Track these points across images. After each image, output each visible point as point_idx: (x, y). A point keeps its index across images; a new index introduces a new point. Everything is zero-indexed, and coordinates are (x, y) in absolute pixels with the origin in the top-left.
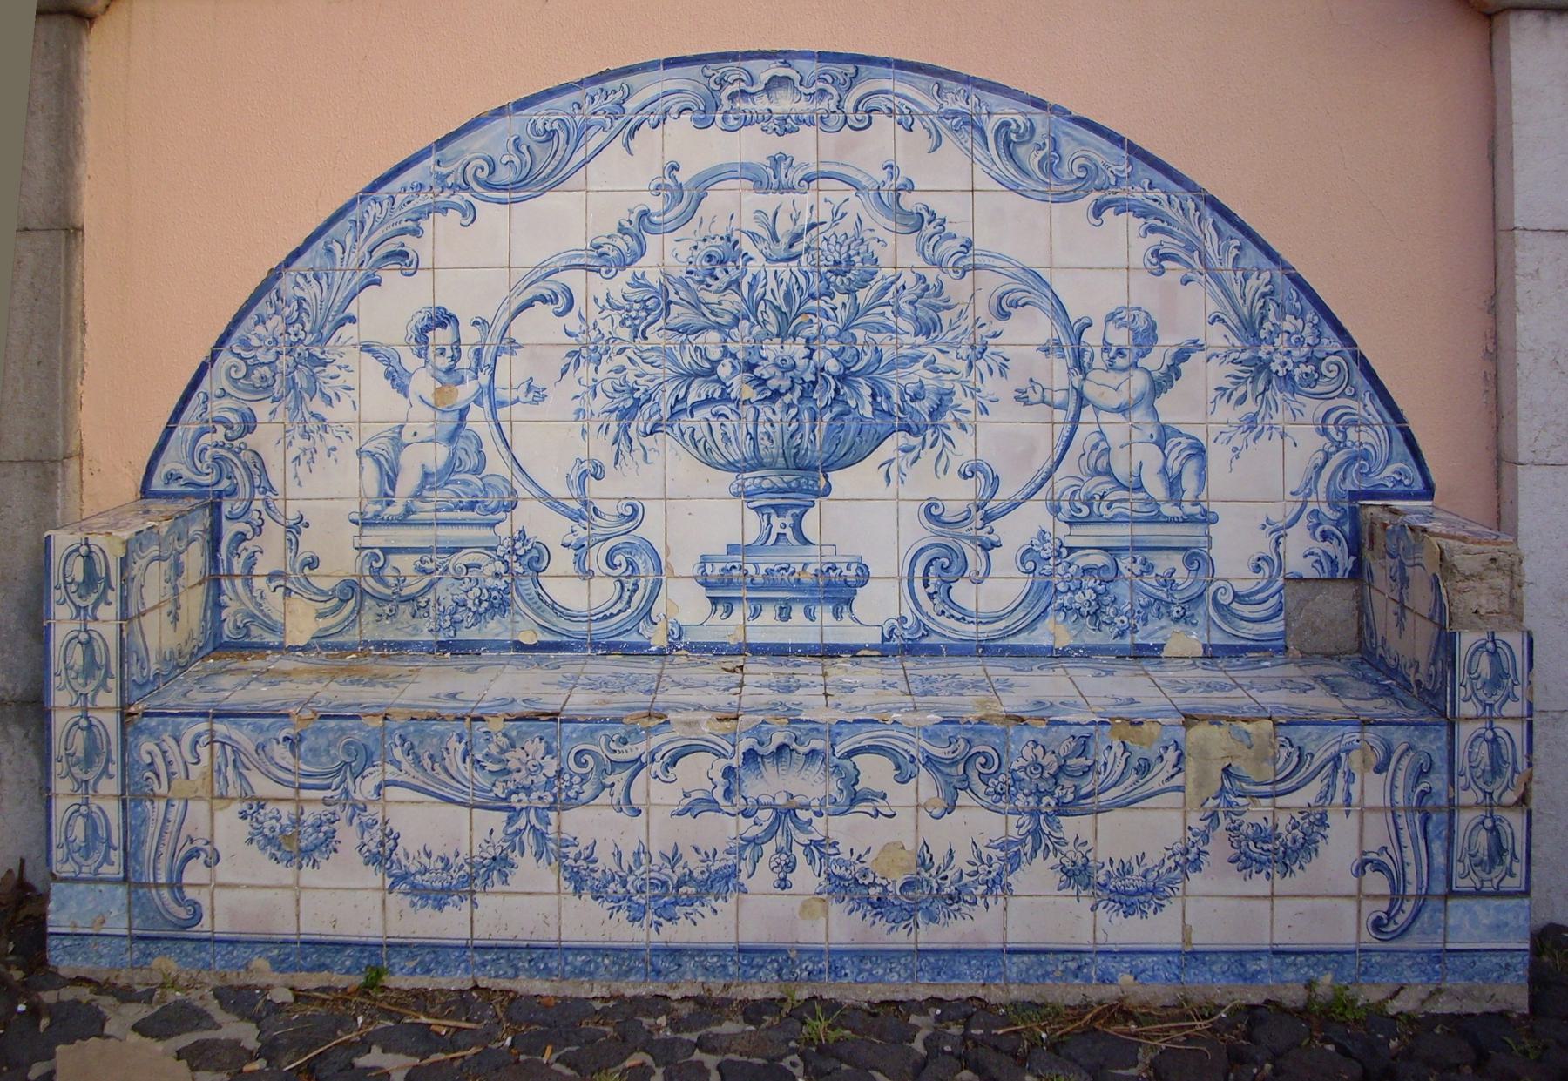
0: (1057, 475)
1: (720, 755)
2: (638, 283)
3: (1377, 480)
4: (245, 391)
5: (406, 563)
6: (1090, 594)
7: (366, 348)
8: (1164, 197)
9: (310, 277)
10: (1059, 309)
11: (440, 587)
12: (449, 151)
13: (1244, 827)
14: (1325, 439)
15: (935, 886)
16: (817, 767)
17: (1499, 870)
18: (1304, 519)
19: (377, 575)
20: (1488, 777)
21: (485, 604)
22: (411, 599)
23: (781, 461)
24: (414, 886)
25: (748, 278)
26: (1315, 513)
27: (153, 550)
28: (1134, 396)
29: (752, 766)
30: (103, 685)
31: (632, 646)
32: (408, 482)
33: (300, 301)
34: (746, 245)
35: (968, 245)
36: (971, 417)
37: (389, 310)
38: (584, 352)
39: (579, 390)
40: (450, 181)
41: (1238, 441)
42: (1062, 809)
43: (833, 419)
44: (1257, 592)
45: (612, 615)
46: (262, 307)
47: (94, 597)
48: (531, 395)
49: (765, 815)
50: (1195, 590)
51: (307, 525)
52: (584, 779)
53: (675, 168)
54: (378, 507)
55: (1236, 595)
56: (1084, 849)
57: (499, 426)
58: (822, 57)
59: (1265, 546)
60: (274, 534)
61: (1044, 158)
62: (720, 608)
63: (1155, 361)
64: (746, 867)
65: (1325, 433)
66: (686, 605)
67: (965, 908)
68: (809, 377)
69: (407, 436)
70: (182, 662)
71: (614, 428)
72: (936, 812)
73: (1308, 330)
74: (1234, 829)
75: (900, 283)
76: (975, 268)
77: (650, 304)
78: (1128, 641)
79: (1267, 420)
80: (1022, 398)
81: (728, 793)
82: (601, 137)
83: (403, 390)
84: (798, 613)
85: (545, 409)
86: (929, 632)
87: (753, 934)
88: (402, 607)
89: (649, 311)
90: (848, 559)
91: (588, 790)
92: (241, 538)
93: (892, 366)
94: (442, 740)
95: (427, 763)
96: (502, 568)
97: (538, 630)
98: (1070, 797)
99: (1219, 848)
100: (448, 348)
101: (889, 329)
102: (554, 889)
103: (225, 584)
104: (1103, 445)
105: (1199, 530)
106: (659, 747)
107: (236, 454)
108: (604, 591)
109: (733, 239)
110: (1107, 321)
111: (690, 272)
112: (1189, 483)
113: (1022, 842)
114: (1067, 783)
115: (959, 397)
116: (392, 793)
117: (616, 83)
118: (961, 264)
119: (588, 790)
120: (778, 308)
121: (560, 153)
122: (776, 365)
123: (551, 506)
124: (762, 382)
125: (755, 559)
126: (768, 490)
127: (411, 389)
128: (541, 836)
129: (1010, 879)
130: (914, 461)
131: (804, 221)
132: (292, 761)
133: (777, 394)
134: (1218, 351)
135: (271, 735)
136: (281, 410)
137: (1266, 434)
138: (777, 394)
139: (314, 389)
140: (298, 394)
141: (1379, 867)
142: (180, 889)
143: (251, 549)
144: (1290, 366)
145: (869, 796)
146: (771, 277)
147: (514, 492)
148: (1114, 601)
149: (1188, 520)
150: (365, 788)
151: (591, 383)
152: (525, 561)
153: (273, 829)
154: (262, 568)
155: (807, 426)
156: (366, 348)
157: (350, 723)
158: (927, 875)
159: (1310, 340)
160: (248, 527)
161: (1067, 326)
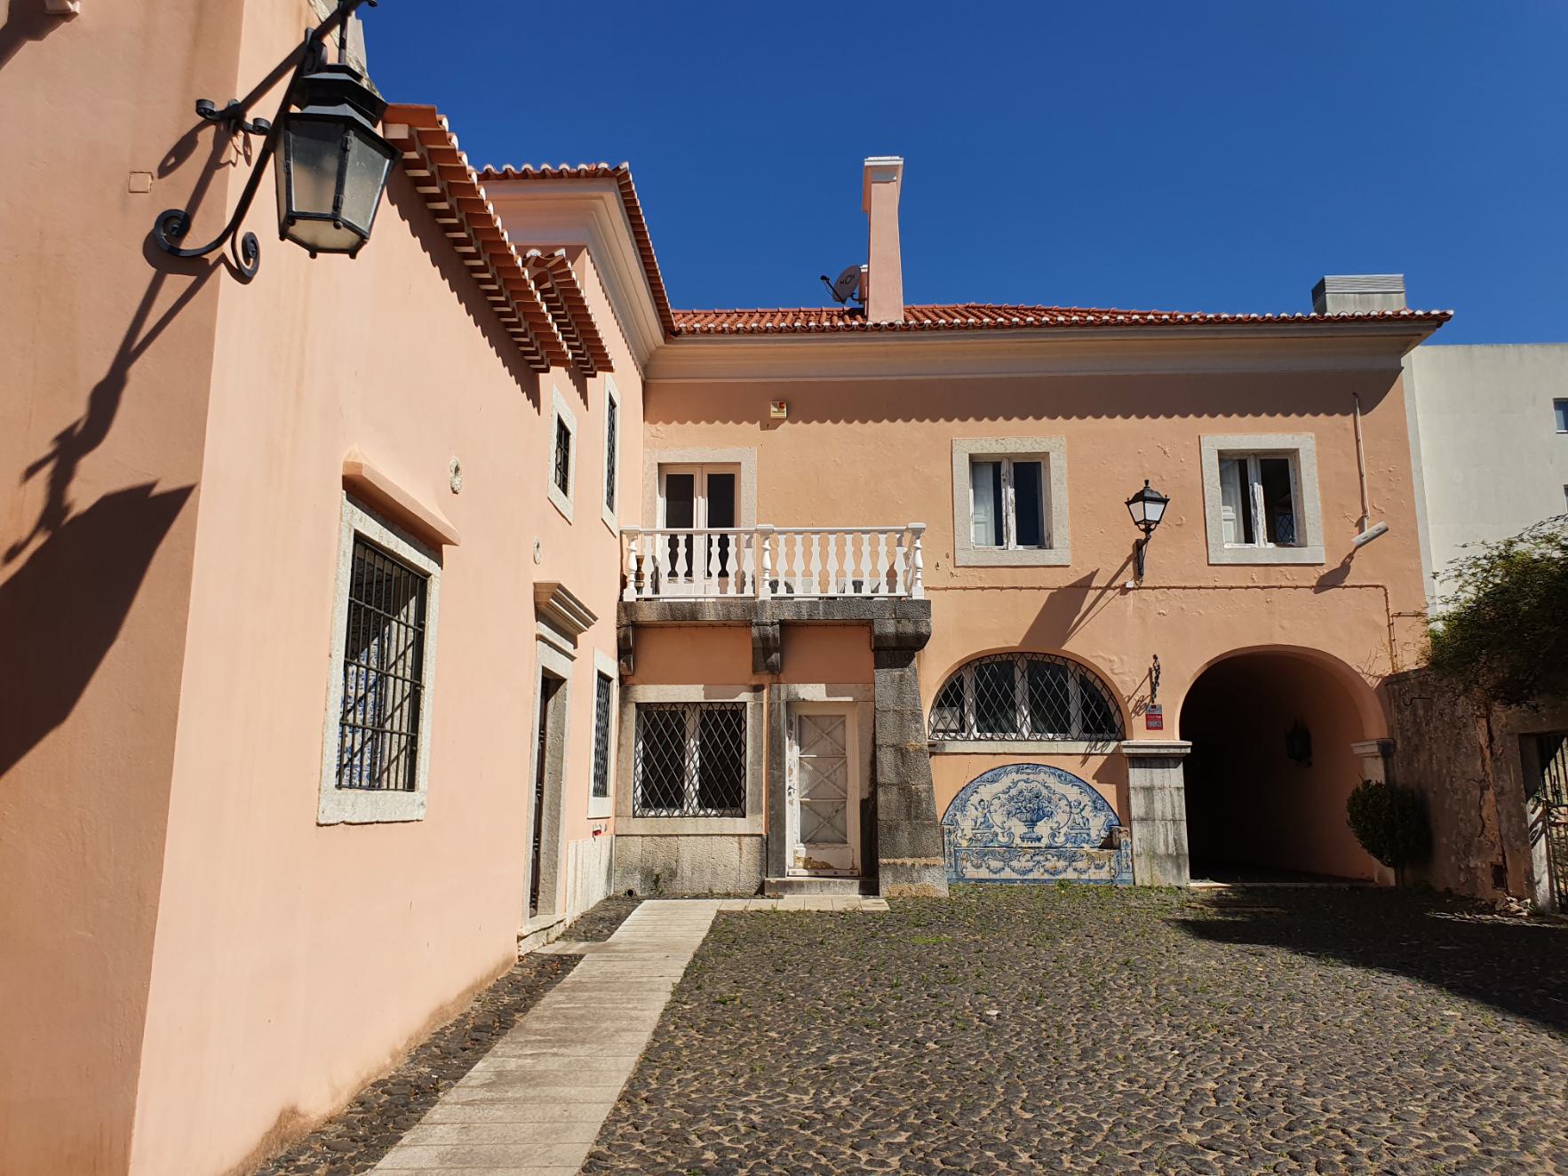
37: (975, 799)
66: (1018, 841)
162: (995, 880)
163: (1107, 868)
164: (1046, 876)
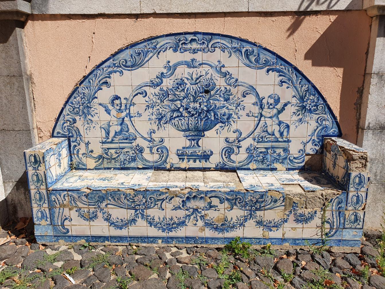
0: (255, 132)
1: (181, 198)
2: (161, 90)
3: (329, 133)
4: (73, 114)
5: (113, 151)
6: (261, 157)
7: (100, 104)
8: (284, 67)
9: (86, 88)
10: (257, 95)
11: (121, 156)
12: (116, 57)
13: (297, 214)
14: (317, 124)
15: (228, 225)
16: (202, 201)
17: (356, 224)
18: (311, 142)
19: (107, 154)
20: (355, 204)
21: (131, 160)
22: (114, 159)
23: (194, 129)
24: (115, 225)
25: (186, 89)
26: (314, 140)
27: (52, 153)
28: (274, 114)
29: (188, 200)
30: (42, 184)
31: (163, 168)
32: (112, 134)
33: (84, 93)
34: (186, 81)
35: (237, 80)
36: (236, 119)
37: (104, 95)
38: (150, 106)
39: (149, 114)
40: (116, 65)
41: (297, 124)
42: (257, 209)
43: (205, 120)
44: (299, 157)
45: (158, 162)
46: (75, 95)
47: (37, 165)
48: (138, 115)
49: (191, 210)
50: (285, 157)
51: (90, 143)
52: (152, 203)
53: (169, 62)
54: (106, 139)
55: (294, 157)
56: (261, 218)
57: (131, 122)
58: (204, 34)
59: (302, 147)
60: (83, 146)
61: (256, 58)
62: (181, 160)
63: (279, 106)
64: (187, 221)
65: (317, 122)
67: (235, 230)
68: (200, 111)
69: (111, 124)
70: (63, 175)
71: (157, 122)
72: (229, 210)
73: (316, 99)
74: (295, 214)
75: (221, 89)
76: (239, 85)
77: (164, 95)
78: (269, 167)
79: (304, 119)
80: (248, 115)
81: (183, 206)
82: (151, 54)
83: (109, 114)
84: (198, 161)
85: (141, 118)
86: (226, 165)
87: (189, 234)
88: (112, 160)
89: (164, 96)
90: (208, 150)
91: (153, 205)
92: (75, 146)
93: (218, 108)
94: (120, 195)
95: (117, 200)
96: (134, 152)
97: (142, 165)
98: (259, 207)
99: (292, 217)
100: (119, 104)
101: (218, 100)
102: (146, 225)
103: (73, 156)
104: (266, 125)
105: (287, 144)
106: (168, 196)
107: (73, 128)
108: (156, 157)
109: (183, 79)
110: (268, 97)
111: (173, 87)
112: (285, 133)
113: (248, 216)
114: (258, 204)
115: (233, 115)
116: (109, 206)
117: (154, 41)
118: (235, 85)
119: (153, 205)
120: (193, 96)
121: (142, 58)
122: (192, 108)
123: (144, 139)
124: (190, 112)
125: (188, 150)
126: (191, 136)
127: (111, 114)
128: (143, 215)
129: (245, 224)
130: (223, 129)
131: (199, 75)
132: (86, 200)
133: (193, 115)
134: (294, 104)
135: (81, 194)
136: (82, 118)
137: (304, 123)
138: (193, 115)
139: (89, 114)
140: (85, 115)
141: (328, 222)
142: (64, 226)
143: (78, 149)
144: (311, 107)
145: (214, 206)
146: (191, 88)
147: (136, 136)
148: (267, 159)
149: (285, 141)
150: (103, 205)
151: (152, 113)
152: (139, 150)
153: (83, 214)
154: (81, 152)
155: (199, 122)
156: (100, 104)
157: (99, 192)
158: (226, 223)
159: (316, 101)
160: (77, 144)
161: (259, 98)
162: (120, 239)
163: (317, 221)
164: (208, 233)
